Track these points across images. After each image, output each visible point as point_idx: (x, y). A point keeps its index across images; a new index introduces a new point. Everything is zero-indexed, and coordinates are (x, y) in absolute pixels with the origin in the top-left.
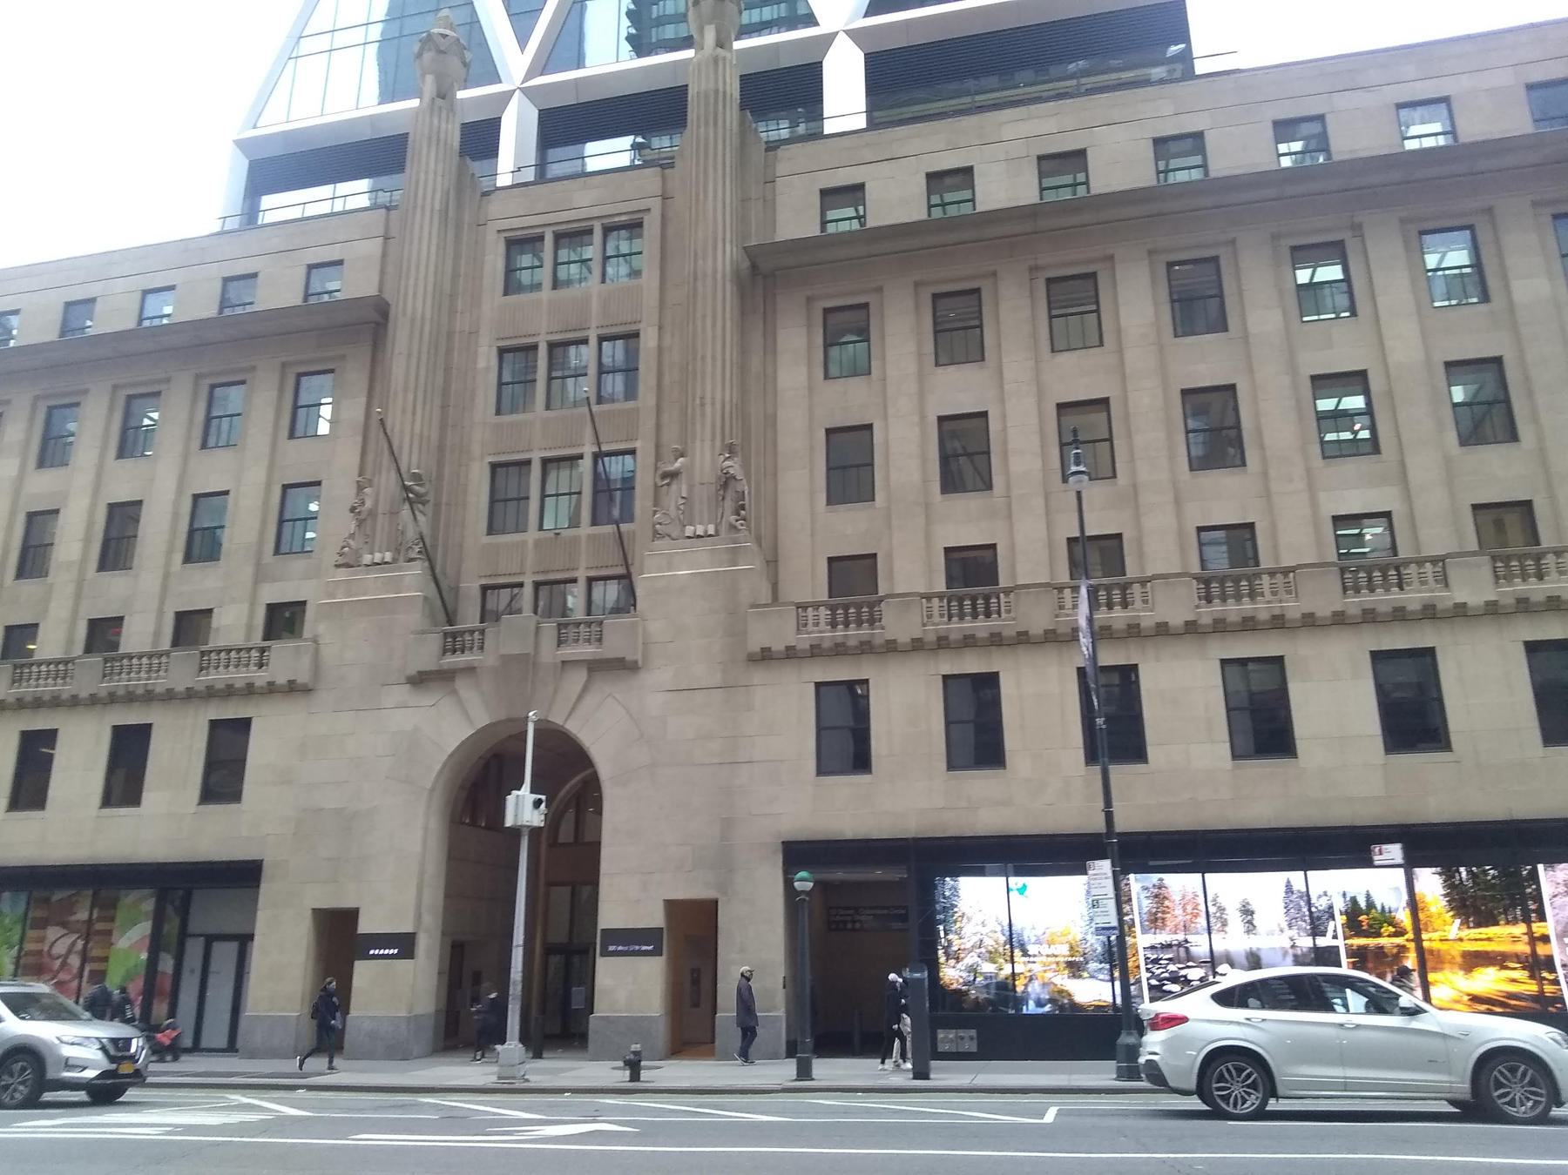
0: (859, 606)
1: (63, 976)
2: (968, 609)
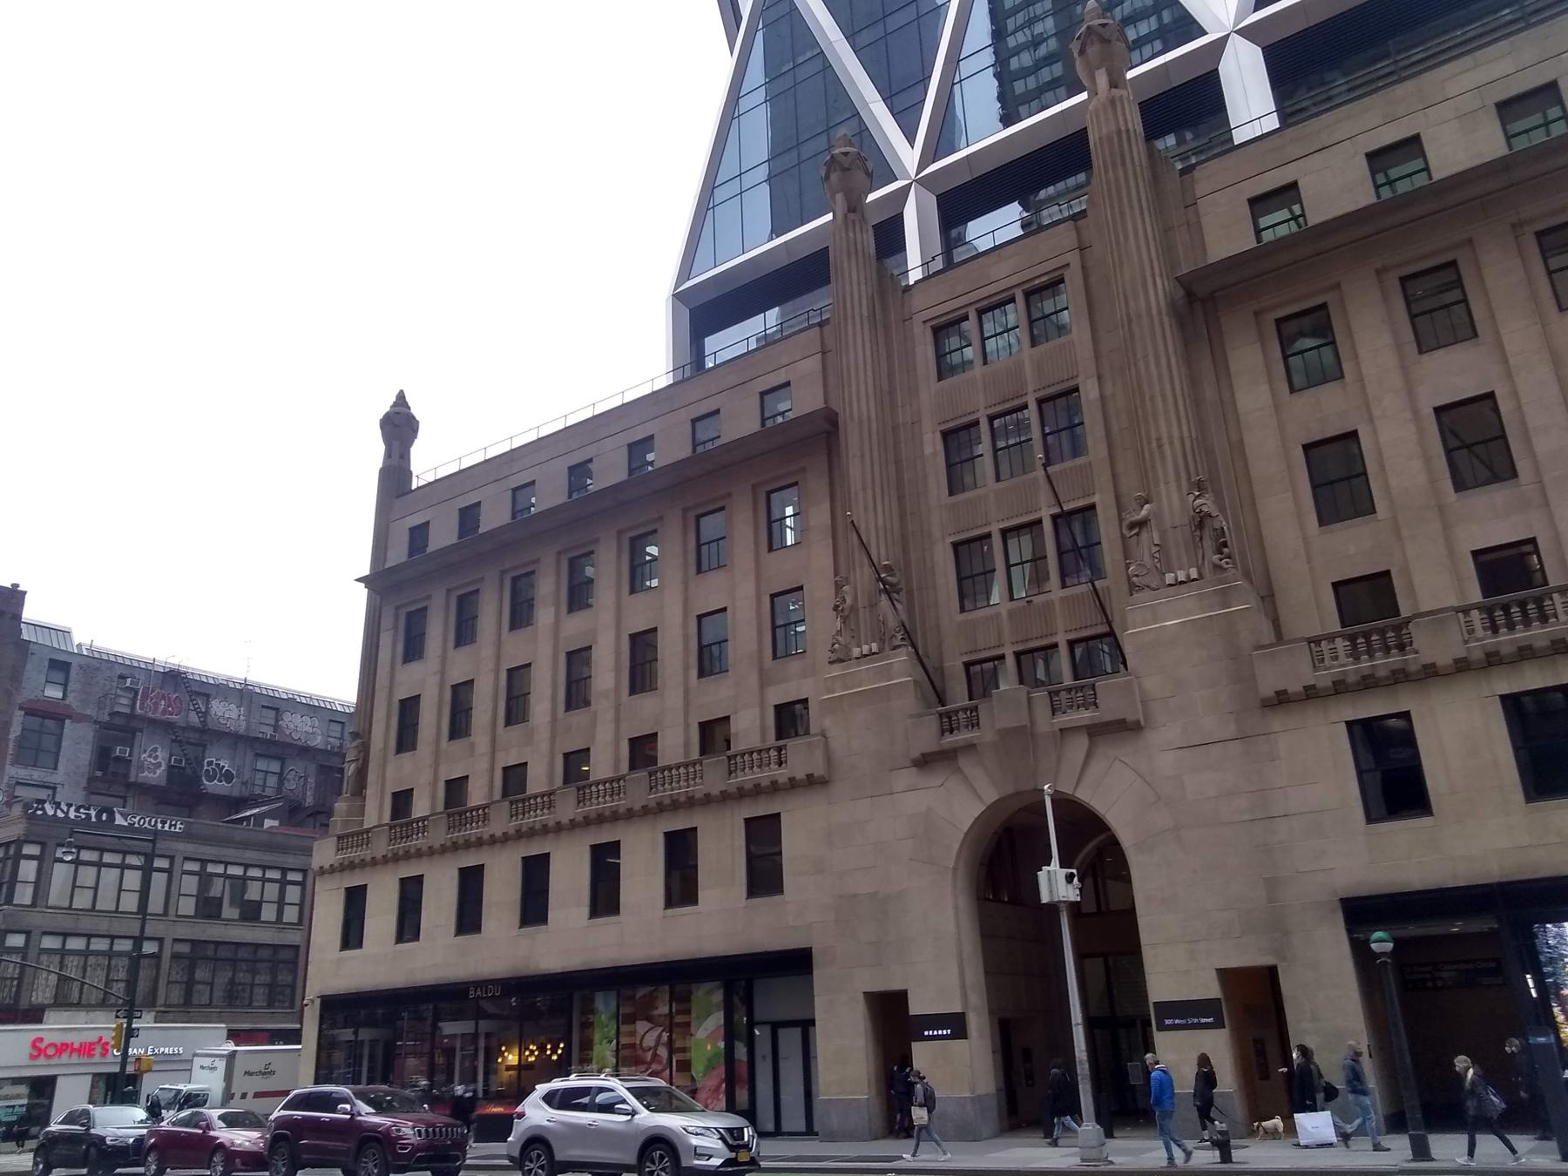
0: (1382, 632)
1: (654, 1067)
2: (1517, 617)
